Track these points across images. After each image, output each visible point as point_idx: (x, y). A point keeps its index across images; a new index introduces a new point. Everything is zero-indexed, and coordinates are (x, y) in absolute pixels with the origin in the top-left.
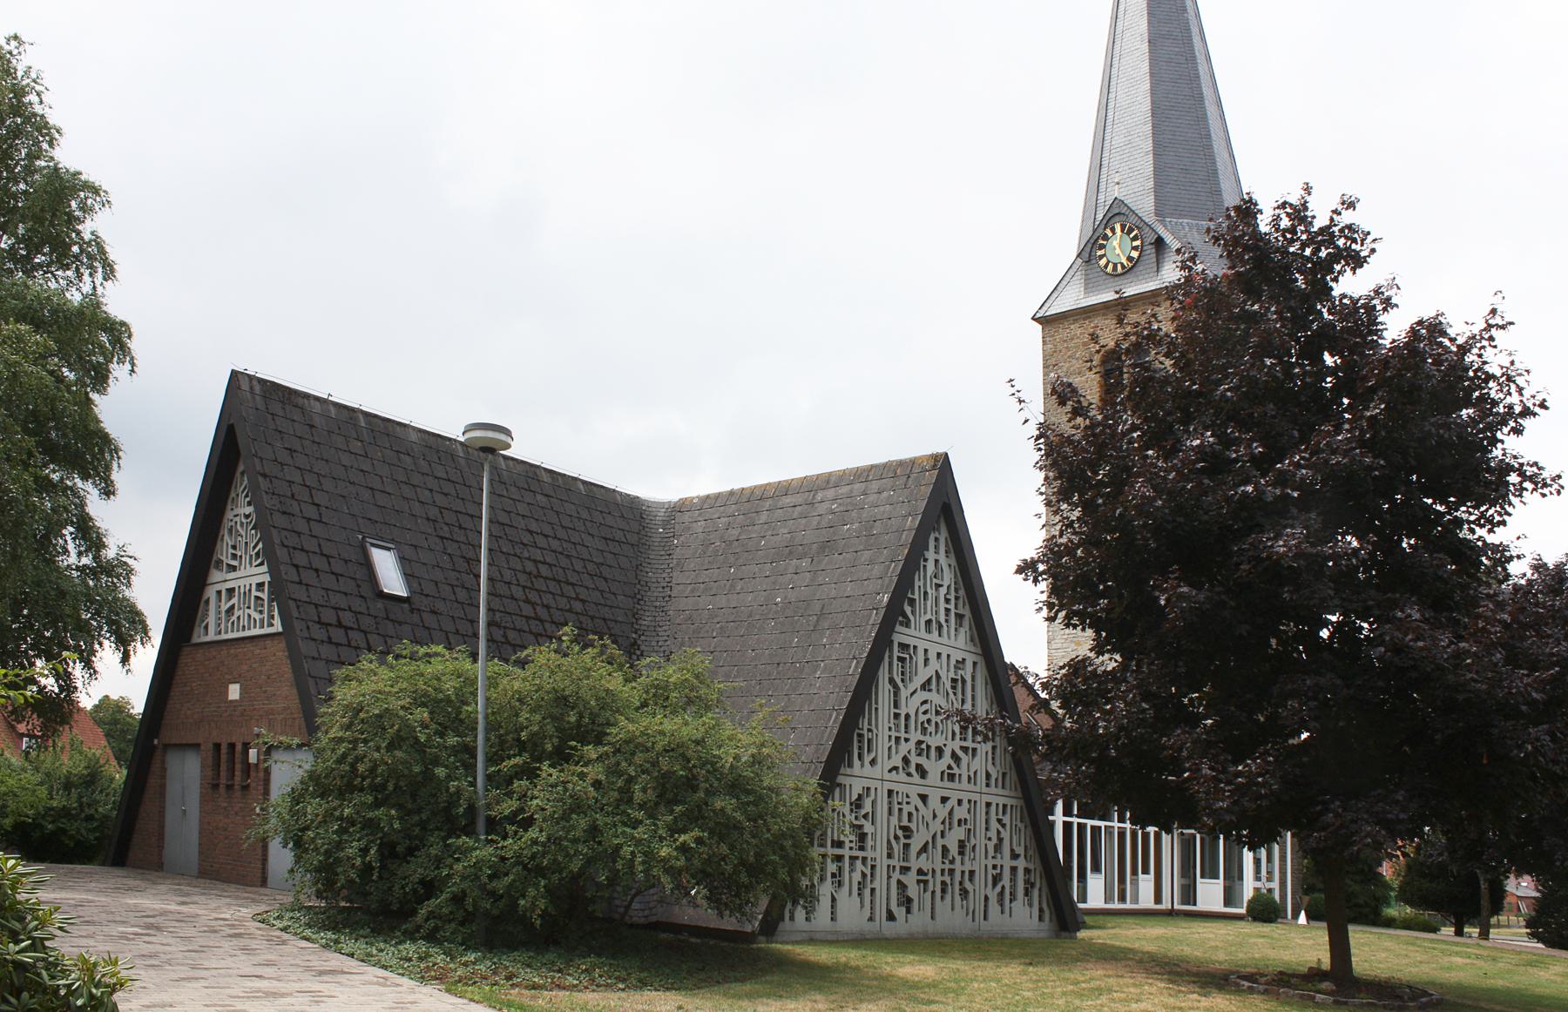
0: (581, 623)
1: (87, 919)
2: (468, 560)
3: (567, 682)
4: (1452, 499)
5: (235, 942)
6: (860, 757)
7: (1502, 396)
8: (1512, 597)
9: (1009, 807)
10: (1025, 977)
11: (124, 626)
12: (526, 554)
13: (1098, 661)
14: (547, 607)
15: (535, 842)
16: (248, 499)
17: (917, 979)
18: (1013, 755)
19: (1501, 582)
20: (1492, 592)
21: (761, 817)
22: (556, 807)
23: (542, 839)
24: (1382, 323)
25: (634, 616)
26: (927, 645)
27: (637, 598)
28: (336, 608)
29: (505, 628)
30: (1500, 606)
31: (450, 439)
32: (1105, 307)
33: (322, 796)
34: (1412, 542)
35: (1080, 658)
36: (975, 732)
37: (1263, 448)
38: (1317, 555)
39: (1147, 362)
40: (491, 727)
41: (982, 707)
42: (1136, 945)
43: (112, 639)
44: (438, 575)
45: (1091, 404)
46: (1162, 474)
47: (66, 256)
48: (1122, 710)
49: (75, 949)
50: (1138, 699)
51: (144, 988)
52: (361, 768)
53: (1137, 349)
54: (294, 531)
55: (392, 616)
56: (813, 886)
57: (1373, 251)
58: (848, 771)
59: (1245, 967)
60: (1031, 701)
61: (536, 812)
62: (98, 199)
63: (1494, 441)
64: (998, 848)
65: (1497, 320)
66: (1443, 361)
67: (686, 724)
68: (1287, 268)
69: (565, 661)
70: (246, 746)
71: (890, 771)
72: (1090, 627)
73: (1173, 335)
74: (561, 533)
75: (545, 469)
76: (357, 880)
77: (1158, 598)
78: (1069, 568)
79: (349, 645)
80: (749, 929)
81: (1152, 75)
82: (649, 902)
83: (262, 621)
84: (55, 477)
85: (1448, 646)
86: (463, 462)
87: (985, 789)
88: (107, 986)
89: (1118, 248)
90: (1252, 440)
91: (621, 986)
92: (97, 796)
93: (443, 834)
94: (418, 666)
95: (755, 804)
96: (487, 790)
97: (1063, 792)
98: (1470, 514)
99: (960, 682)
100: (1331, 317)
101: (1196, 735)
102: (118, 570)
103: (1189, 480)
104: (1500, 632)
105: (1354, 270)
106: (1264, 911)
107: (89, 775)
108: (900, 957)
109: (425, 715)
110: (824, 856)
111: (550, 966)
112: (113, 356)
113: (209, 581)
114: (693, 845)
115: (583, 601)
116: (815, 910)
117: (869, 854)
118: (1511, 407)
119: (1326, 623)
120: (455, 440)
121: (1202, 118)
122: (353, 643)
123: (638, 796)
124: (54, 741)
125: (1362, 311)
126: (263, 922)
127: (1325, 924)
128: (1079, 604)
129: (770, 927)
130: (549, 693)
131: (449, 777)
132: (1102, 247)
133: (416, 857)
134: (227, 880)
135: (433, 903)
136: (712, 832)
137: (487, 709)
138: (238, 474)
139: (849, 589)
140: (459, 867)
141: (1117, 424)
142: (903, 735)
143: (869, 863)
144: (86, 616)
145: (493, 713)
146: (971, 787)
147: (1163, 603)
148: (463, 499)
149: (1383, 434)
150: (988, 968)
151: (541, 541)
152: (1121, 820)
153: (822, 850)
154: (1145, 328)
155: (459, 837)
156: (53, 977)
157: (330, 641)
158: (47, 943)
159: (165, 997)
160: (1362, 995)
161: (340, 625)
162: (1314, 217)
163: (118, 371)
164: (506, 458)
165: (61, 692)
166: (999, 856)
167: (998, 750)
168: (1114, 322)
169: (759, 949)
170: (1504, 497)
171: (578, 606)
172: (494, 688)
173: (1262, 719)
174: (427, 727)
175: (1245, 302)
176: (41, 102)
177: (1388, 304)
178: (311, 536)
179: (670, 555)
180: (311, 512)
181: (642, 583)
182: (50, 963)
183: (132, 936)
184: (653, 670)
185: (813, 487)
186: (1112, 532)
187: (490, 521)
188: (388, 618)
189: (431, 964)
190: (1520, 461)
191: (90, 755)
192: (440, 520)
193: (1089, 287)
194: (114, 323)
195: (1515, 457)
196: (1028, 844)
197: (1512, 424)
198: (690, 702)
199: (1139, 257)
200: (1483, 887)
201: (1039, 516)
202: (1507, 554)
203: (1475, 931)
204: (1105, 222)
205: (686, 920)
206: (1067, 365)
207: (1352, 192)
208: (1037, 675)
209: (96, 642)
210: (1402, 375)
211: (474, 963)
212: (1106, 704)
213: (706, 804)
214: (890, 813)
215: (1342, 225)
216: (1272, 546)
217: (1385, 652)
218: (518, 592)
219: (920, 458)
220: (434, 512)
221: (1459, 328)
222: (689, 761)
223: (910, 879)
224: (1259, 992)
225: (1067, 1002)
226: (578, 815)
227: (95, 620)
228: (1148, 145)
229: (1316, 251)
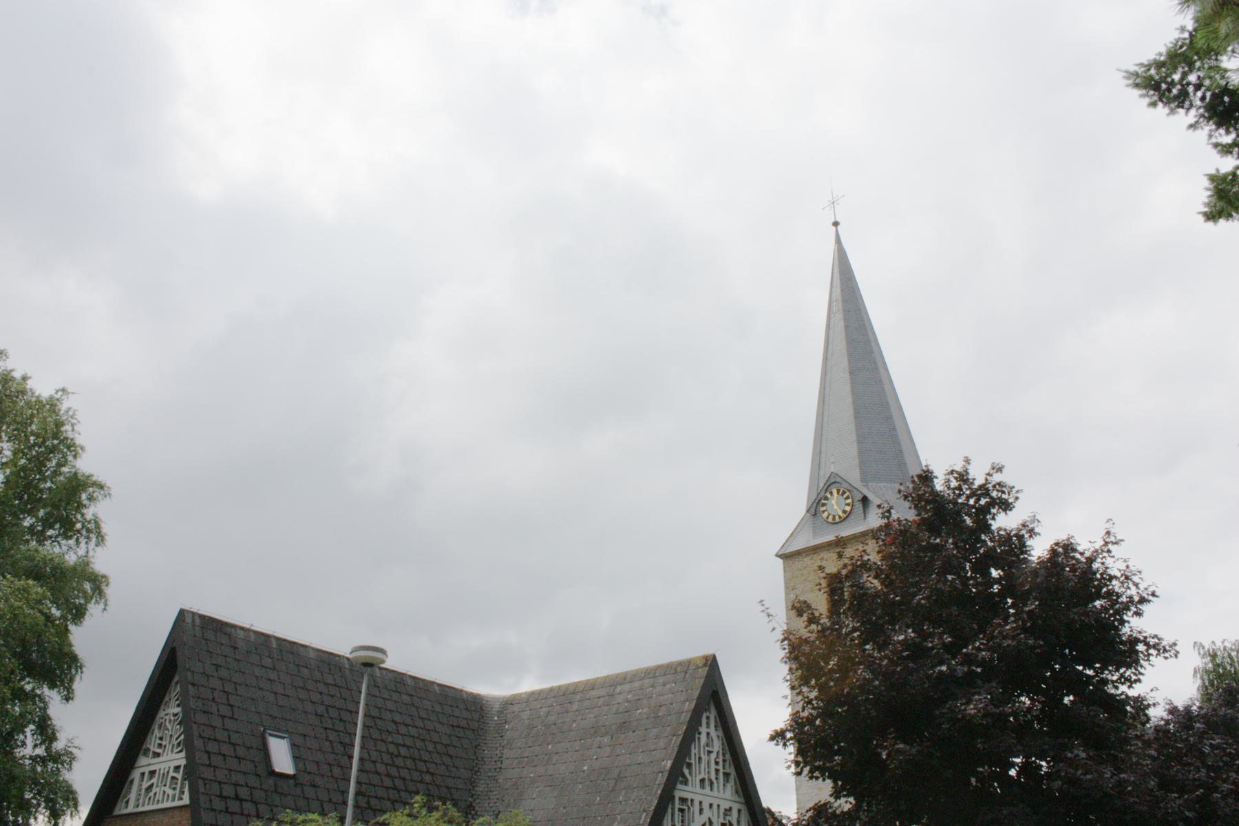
0: (429, 790)
2: (344, 745)
11: (59, 803)
12: (390, 739)
13: (836, 805)
14: (404, 779)
16: (178, 702)
24: (1029, 546)
25: (471, 785)
27: (475, 770)
29: (369, 796)
30: (1147, 744)
31: (339, 656)
35: (822, 803)
37: (952, 637)
38: (1000, 714)
44: (320, 757)
45: (821, 614)
46: (877, 661)
55: (279, 790)
57: (1017, 498)
62: (102, 492)
63: (1122, 622)
65: (1112, 539)
68: (958, 513)
72: (829, 777)
74: (419, 723)
75: (410, 676)
77: (879, 755)
79: (242, 814)
83: (174, 796)
84: (28, 688)
85: (1111, 777)
86: (347, 672)
89: (836, 505)
90: (944, 633)
99: (707, 780)
103: (897, 665)
104: (1151, 764)
112: (92, 598)
113: (137, 765)
115: (432, 774)
119: (1013, 765)
120: (343, 657)
122: (246, 812)
128: (820, 761)
132: (824, 505)
138: (173, 684)
139: (640, 758)
144: (28, 796)
147: (884, 757)
154: (859, 560)
157: (227, 811)
161: (237, 798)
162: (974, 479)
163: (94, 609)
170: (1137, 662)
171: (428, 778)
175: (930, 538)
176: (73, 430)
177: (1032, 532)
179: (502, 737)
180: (225, 710)
185: (612, 684)
187: (365, 715)
188: (276, 791)
190: (1144, 635)
192: (325, 715)
193: (815, 532)
194: (97, 576)
195: (1140, 632)
201: (785, 697)
202: (1145, 703)
207: (999, 460)
208: (789, 818)
210: (1048, 581)
215: (994, 483)
216: (965, 710)
217: (1062, 785)
219: (694, 659)
220: (321, 709)
221: (1086, 544)
228: (854, 437)
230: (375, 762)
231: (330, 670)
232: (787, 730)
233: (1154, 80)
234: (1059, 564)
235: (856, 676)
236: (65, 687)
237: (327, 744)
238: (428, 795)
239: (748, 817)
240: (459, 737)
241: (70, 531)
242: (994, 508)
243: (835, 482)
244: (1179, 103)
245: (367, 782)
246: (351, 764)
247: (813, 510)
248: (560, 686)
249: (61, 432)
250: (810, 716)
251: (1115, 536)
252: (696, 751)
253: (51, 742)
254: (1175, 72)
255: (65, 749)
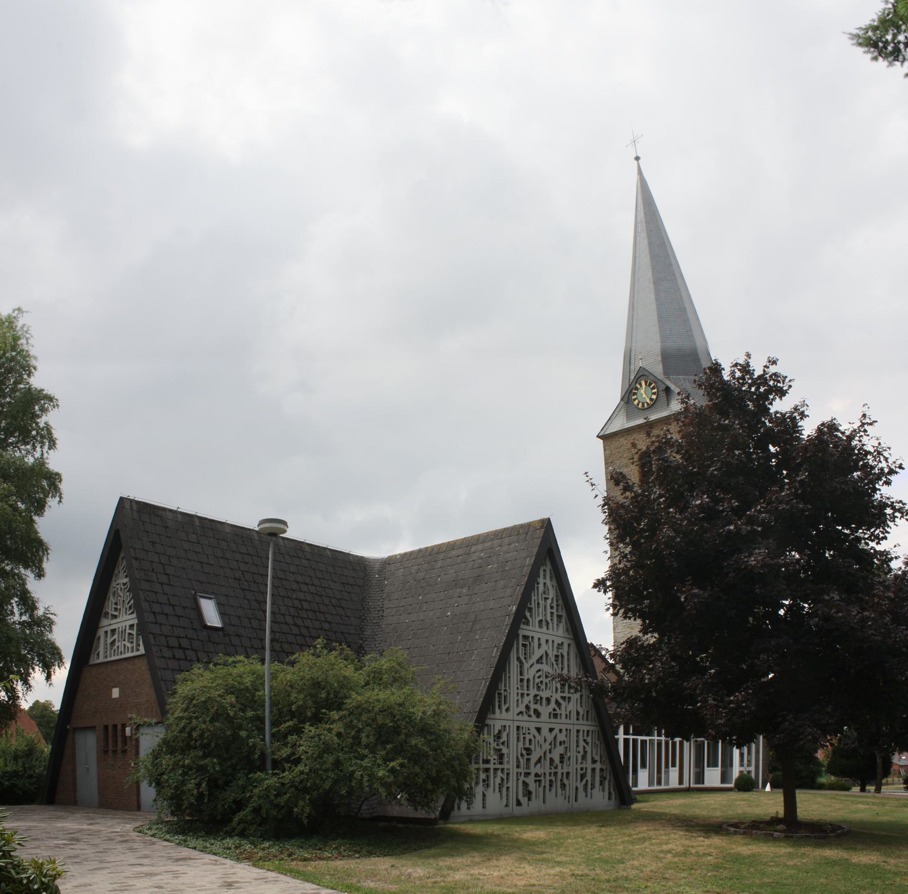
0: (328, 636)
1: (34, 837)
2: (259, 602)
3: (320, 673)
4: (853, 526)
5: (124, 845)
6: (500, 707)
7: (876, 463)
8: (894, 582)
9: (591, 732)
10: (599, 834)
12: (294, 596)
14: (307, 628)
15: (302, 773)
16: (125, 574)
17: (534, 840)
18: (593, 699)
19: (886, 574)
20: (881, 580)
21: (439, 748)
22: (314, 750)
23: (307, 771)
24: (801, 426)
25: (360, 630)
26: (539, 635)
28: (178, 637)
29: (282, 642)
30: (887, 588)
31: (249, 530)
32: (639, 428)
33: (171, 753)
34: (831, 553)
35: (633, 637)
36: (570, 687)
37: (738, 502)
39: (665, 457)
40: (273, 704)
41: (573, 670)
42: (667, 811)
43: (40, 665)
45: (634, 484)
46: (679, 522)
47: (28, 437)
48: (659, 668)
49: (29, 856)
50: (669, 660)
51: (73, 876)
52: (195, 734)
53: (660, 450)
54: (153, 592)
56: (471, 788)
57: (790, 386)
58: (493, 716)
59: (732, 819)
60: (603, 665)
61: (302, 754)
62: (51, 404)
63: (875, 490)
64: (584, 757)
65: (867, 420)
66: (839, 445)
67: (393, 694)
68: (742, 399)
69: (318, 660)
70: (124, 726)
71: (518, 714)
72: (639, 617)
73: (680, 441)
75: (308, 544)
76: (195, 803)
77: (680, 597)
78: (625, 583)
79: (186, 659)
80: (433, 816)
81: (656, 300)
82: (372, 805)
83: (132, 648)
84: (8, 568)
85: (857, 615)
87: (576, 722)
88: (51, 876)
89: (644, 394)
90: (731, 498)
91: (357, 855)
92: (34, 763)
93: (246, 772)
94: (228, 669)
95: (436, 740)
96: (272, 743)
97: (623, 720)
98: (865, 534)
100: (771, 425)
101: (704, 680)
102: (46, 623)
103: (695, 525)
104: (888, 604)
105: (781, 398)
106: (746, 784)
107: (28, 750)
108: (524, 827)
109: (233, 699)
110: (478, 769)
111: (314, 846)
112: (49, 493)
114: (398, 768)
115: (329, 623)
116: (473, 802)
117: (505, 766)
118: (882, 469)
119: (782, 606)
120: (253, 530)
121: (686, 321)
122: (189, 658)
123: (364, 740)
124: (6, 731)
125: (788, 420)
126: (140, 832)
127: (781, 790)
128: (632, 604)
129: (446, 814)
130: (308, 680)
131: (249, 737)
132: (635, 394)
133: (230, 787)
134: (117, 808)
135: (242, 814)
136: (410, 760)
137: (271, 693)
138: (120, 559)
140: (256, 791)
141: (650, 494)
142: (526, 692)
143: (506, 771)
144: (24, 652)
145: (275, 695)
146: (568, 721)
148: (256, 565)
149: (809, 489)
150: (577, 830)
151: (304, 588)
152: (659, 735)
153: (477, 766)
154: (663, 438)
155: (255, 773)
156: (18, 873)
157: (174, 658)
158: (12, 853)
159: (86, 880)
160: (801, 831)
161: (180, 647)
162: (754, 370)
163: (52, 502)
164: (284, 538)
165: (9, 699)
166: (584, 762)
167: (584, 697)
168: (645, 435)
169: (440, 828)
171: (326, 626)
172: (276, 680)
173: (745, 667)
174: (234, 707)
175: (720, 419)
176: (27, 343)
177: (803, 415)
178: (164, 593)
180: (164, 579)
181: (366, 609)
182: (15, 865)
183: (62, 846)
184: (374, 662)
185: (468, 544)
186: (650, 559)
187: (273, 577)
188: (210, 641)
189: (243, 850)
190: (891, 500)
191: (28, 738)
193: (629, 417)
195: (888, 498)
196: (602, 754)
197: (884, 479)
198: (395, 680)
199: (657, 398)
200: (878, 761)
201: (606, 552)
202: (889, 556)
203: (872, 788)
204: (635, 380)
205: (395, 814)
206: (619, 462)
207: (773, 355)
208: (607, 649)
209: (30, 668)
211: (268, 848)
212: (649, 664)
213: (406, 742)
214: (518, 740)
215: (770, 373)
216: (747, 561)
218: (289, 620)
219: (534, 522)
221: (846, 426)
222: (395, 717)
223: (531, 780)
224: (740, 834)
225: (624, 847)
226: (328, 754)
227: (30, 654)
229: (758, 389)
230: (284, 615)
231: (243, 542)
232: (607, 579)
233: (872, 40)
234: (825, 441)
235: (662, 534)
236: (36, 567)
237: (245, 601)
238: (327, 639)
239: (576, 650)
240: (349, 592)
241: (27, 438)
242: (771, 394)
243: (643, 375)
244: (895, 57)
245: (280, 631)
246: (266, 617)
247: (626, 399)
248: (427, 548)
249: (18, 345)
250: (625, 568)
251: (870, 418)
252: (536, 598)
253: (33, 611)
254: (887, 34)
255: (44, 616)
